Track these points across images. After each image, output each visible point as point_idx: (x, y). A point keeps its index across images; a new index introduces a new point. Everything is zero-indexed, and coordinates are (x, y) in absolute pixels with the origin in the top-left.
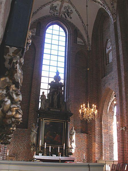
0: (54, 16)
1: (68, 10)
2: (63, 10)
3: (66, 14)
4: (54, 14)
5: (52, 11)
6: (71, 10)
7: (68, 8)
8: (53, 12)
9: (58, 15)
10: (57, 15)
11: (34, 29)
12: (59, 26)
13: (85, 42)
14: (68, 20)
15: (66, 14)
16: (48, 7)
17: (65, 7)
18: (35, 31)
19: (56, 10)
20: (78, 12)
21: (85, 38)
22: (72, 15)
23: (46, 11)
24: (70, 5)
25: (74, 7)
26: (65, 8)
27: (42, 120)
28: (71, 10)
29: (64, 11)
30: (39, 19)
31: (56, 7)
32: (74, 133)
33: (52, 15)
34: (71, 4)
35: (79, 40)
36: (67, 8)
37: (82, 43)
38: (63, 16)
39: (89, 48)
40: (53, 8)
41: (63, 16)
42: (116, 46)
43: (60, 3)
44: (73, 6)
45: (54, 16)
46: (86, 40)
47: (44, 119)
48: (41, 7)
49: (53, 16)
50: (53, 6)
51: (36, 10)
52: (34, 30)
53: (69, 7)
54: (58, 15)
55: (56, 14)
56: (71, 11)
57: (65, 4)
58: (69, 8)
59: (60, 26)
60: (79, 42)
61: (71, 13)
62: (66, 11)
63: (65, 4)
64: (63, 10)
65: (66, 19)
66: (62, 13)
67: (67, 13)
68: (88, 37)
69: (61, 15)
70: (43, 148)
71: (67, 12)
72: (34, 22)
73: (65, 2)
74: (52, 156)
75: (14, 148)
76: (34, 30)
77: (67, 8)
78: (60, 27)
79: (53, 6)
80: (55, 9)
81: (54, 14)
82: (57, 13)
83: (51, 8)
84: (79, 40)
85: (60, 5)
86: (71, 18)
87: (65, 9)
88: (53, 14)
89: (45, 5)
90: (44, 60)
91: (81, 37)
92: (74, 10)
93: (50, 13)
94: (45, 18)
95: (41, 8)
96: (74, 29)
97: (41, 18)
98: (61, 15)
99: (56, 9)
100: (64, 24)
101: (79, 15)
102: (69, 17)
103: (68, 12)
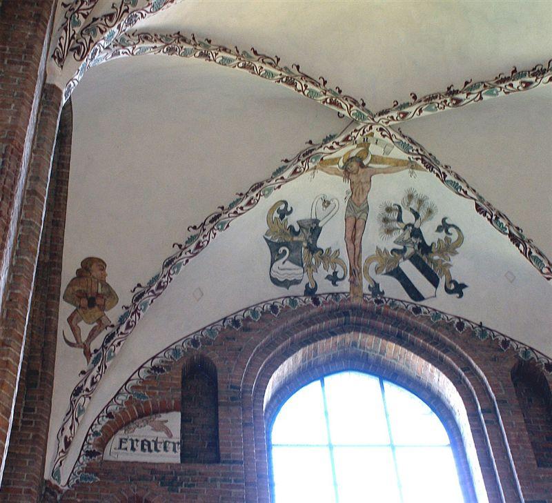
0: (316, 301)
1: (416, 233)
2: (375, 240)
3: (408, 268)
4: (310, 292)
5: (286, 269)
6: (444, 226)
7: (417, 215)
9: (344, 286)
10: (335, 295)
11: (164, 416)
12: (374, 381)
14: (437, 314)
15: (408, 268)
16: (248, 232)
17: (389, 210)
19: (326, 257)
20: (499, 215)
22: (459, 267)
23: (236, 273)
24: (425, 183)
25: (458, 185)
26: (391, 215)
28: (444, 226)
29: (389, 244)
30: (195, 342)
31: (314, 229)
34: (430, 163)
36: (408, 217)
38: (392, 289)
40: (293, 240)
41: (392, 289)
43: (334, 186)
44: (449, 177)
45: (316, 301)
48: (191, 240)
49: (309, 300)
50: (292, 220)
51: (155, 268)
52: (162, 427)
53: (421, 202)
54: (344, 286)
55: (325, 287)
56: (443, 235)
57: (387, 189)
58: (420, 206)
59: (388, 373)
61: (449, 248)
62: (404, 243)
63: (387, 189)
64: (375, 240)
66: (374, 264)
67: (415, 260)
69: (366, 284)
71: (410, 251)
72: (154, 368)
73: (376, 172)
74: (337, 285)
76: (162, 427)
77: (408, 217)
78: (387, 384)
79: (292, 220)
80: (313, 249)
81: (310, 292)
82: (334, 279)
83: (274, 248)
85: (344, 205)
86: (458, 289)
87: (389, 231)
88: (299, 290)
89: (221, 219)
90: (275, 452)
92: (460, 210)
93: (275, 281)
94: (246, 329)
95: (196, 241)
96: (509, 365)
98: (366, 284)
99: (322, 243)
100: (411, 346)
101: (513, 239)
102: (435, 282)
103: (425, 248)
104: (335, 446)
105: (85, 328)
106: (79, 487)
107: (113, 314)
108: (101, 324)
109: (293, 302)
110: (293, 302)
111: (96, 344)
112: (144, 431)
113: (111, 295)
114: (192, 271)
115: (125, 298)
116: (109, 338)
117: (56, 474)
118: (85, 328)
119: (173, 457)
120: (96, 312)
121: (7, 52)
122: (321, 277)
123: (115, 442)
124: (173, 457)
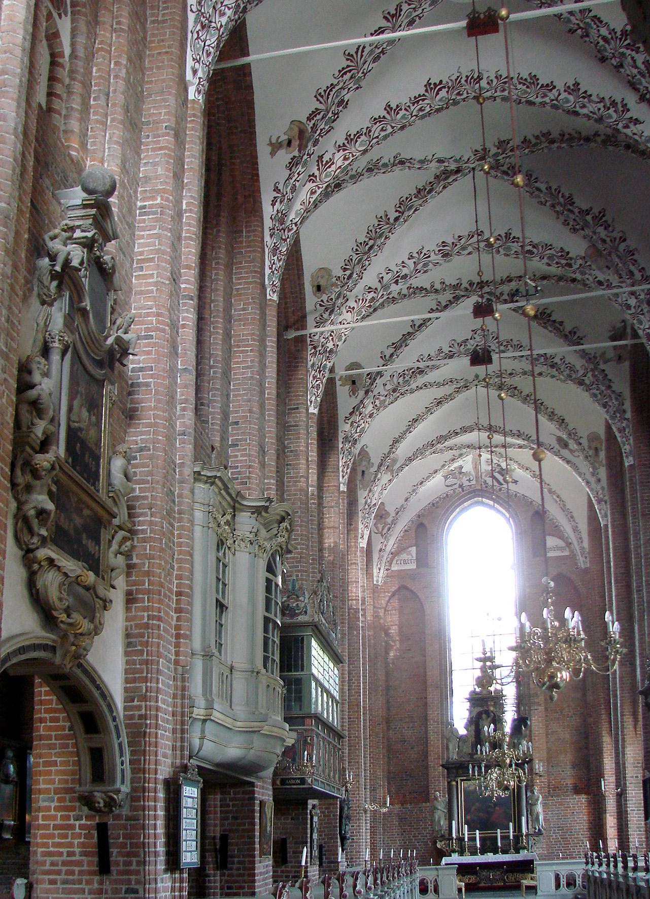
4: (461, 486)
8: (455, 481)
9: (474, 482)
13: (569, 544)
18: (414, 555)
21: (568, 529)
27: (454, 783)
32: (537, 800)
33: (454, 490)
35: (551, 541)
37: (561, 549)
39: (583, 562)
42: (254, 863)
46: (573, 538)
47: (462, 780)
51: (402, 501)
54: (474, 482)
55: (466, 483)
60: (551, 549)
65: (500, 490)
68: (575, 529)
70: (461, 840)
75: (77, 869)
82: (469, 480)
84: (551, 541)
91: (558, 532)
97: (424, 509)
104: (643, 153)
105: (380, 526)
106: (385, 583)
107: (389, 520)
108: (386, 524)
109: (454, 492)
110: (454, 492)
111: (385, 531)
112: (404, 556)
113: (388, 514)
114: (412, 500)
115: (393, 514)
116: (389, 529)
117: (377, 581)
118: (380, 526)
119: (413, 566)
120: (383, 521)
121: (132, 868)
122: (464, 481)
123: (394, 562)
124: (413, 566)
